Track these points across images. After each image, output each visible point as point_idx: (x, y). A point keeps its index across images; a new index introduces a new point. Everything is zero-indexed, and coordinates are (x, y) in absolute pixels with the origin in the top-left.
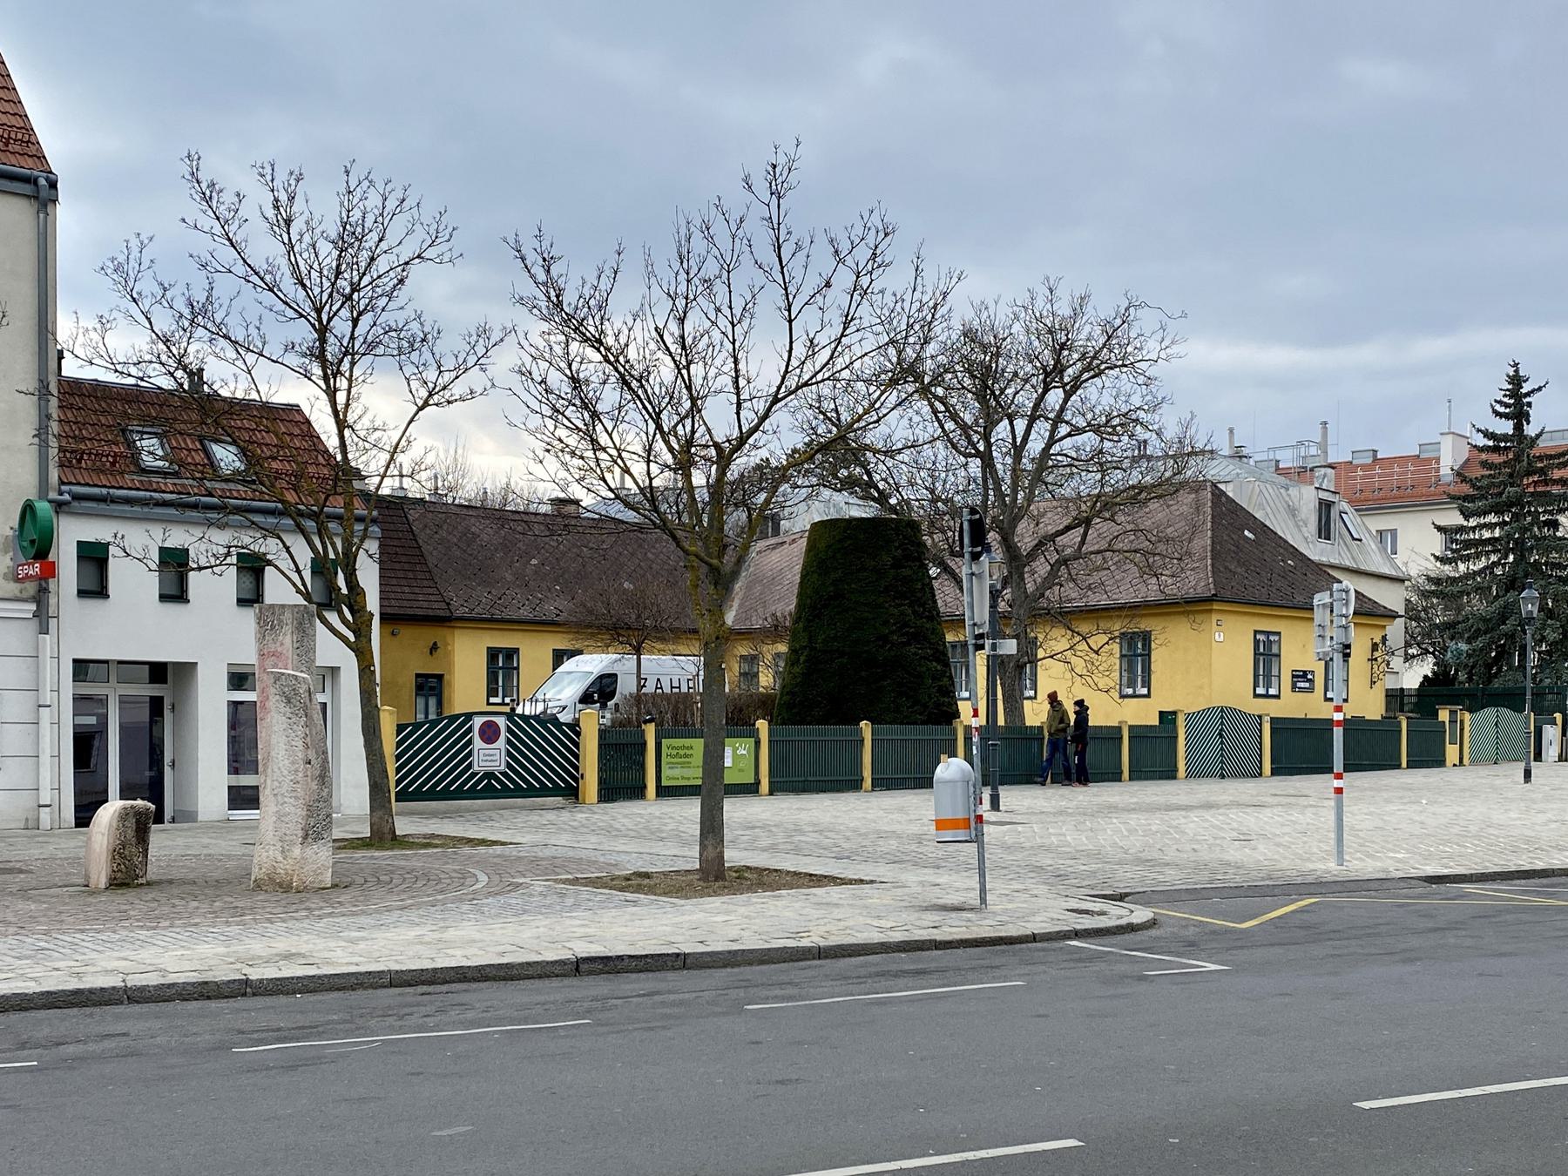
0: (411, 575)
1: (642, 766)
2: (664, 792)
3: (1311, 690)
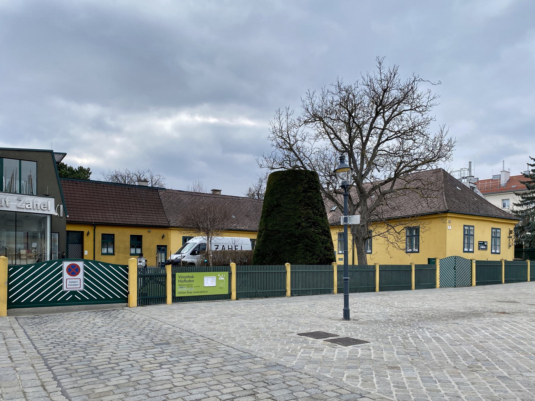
0: (157, 212)
1: (164, 285)
2: (175, 299)
3: (486, 249)
